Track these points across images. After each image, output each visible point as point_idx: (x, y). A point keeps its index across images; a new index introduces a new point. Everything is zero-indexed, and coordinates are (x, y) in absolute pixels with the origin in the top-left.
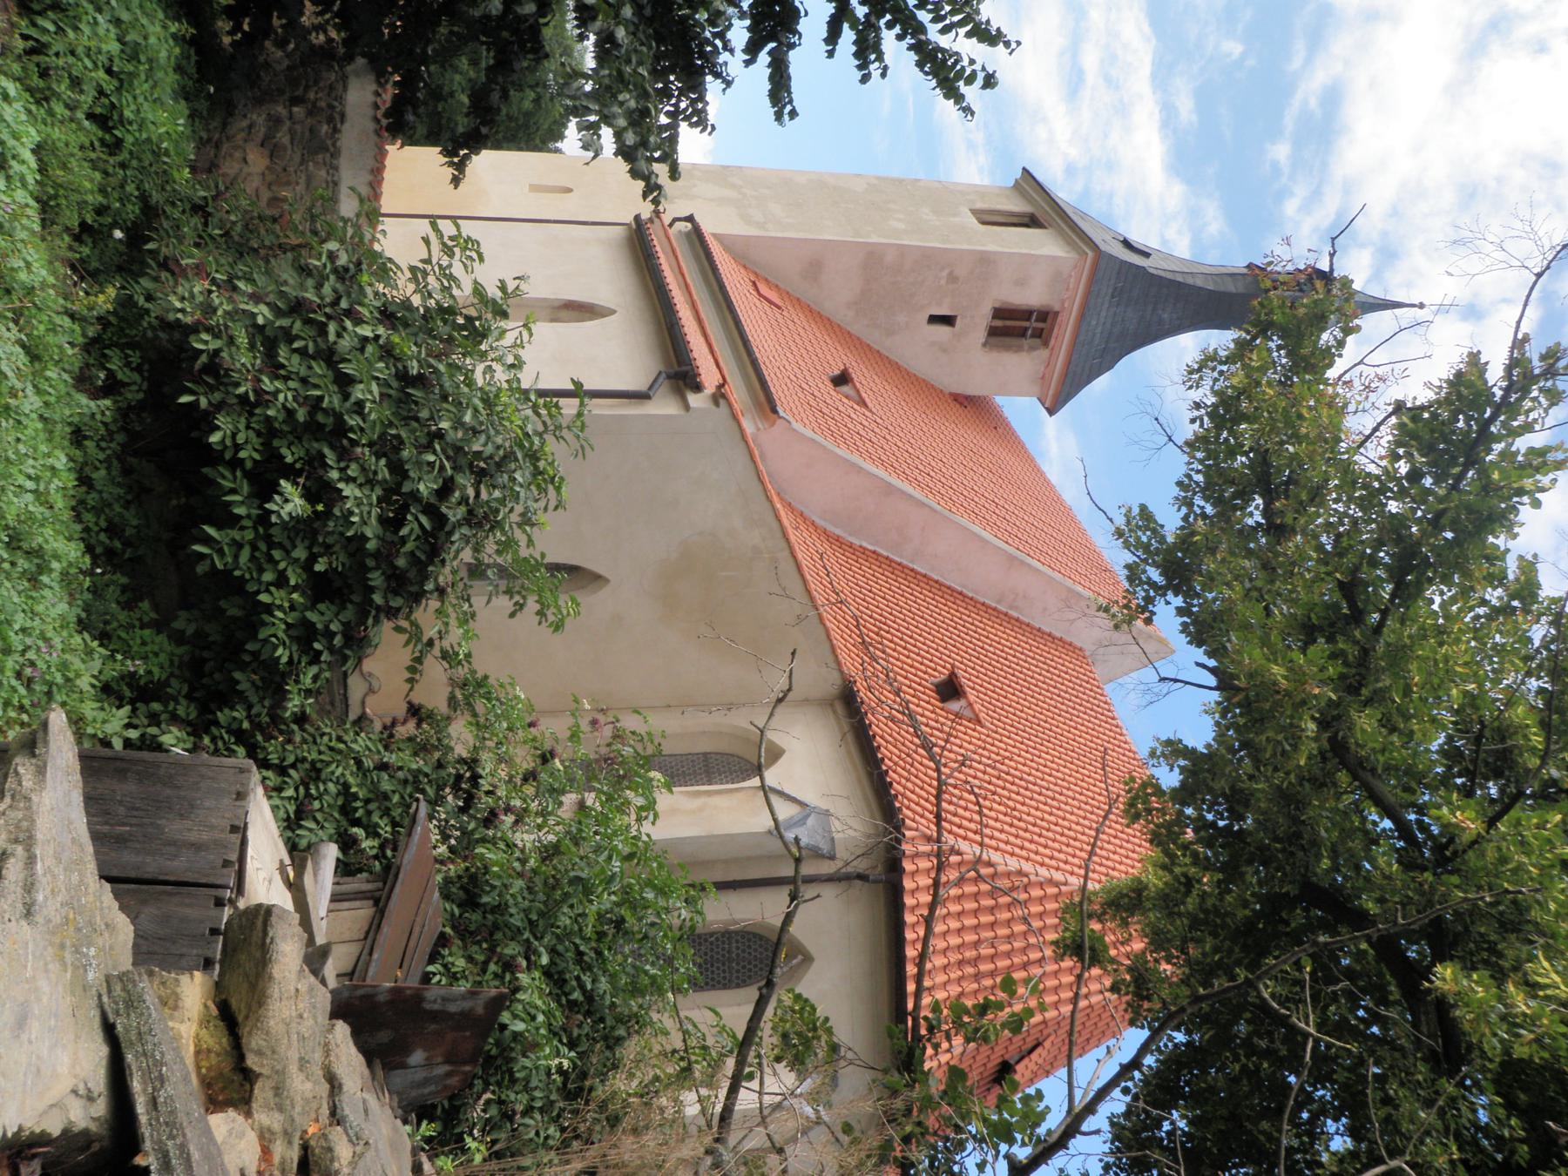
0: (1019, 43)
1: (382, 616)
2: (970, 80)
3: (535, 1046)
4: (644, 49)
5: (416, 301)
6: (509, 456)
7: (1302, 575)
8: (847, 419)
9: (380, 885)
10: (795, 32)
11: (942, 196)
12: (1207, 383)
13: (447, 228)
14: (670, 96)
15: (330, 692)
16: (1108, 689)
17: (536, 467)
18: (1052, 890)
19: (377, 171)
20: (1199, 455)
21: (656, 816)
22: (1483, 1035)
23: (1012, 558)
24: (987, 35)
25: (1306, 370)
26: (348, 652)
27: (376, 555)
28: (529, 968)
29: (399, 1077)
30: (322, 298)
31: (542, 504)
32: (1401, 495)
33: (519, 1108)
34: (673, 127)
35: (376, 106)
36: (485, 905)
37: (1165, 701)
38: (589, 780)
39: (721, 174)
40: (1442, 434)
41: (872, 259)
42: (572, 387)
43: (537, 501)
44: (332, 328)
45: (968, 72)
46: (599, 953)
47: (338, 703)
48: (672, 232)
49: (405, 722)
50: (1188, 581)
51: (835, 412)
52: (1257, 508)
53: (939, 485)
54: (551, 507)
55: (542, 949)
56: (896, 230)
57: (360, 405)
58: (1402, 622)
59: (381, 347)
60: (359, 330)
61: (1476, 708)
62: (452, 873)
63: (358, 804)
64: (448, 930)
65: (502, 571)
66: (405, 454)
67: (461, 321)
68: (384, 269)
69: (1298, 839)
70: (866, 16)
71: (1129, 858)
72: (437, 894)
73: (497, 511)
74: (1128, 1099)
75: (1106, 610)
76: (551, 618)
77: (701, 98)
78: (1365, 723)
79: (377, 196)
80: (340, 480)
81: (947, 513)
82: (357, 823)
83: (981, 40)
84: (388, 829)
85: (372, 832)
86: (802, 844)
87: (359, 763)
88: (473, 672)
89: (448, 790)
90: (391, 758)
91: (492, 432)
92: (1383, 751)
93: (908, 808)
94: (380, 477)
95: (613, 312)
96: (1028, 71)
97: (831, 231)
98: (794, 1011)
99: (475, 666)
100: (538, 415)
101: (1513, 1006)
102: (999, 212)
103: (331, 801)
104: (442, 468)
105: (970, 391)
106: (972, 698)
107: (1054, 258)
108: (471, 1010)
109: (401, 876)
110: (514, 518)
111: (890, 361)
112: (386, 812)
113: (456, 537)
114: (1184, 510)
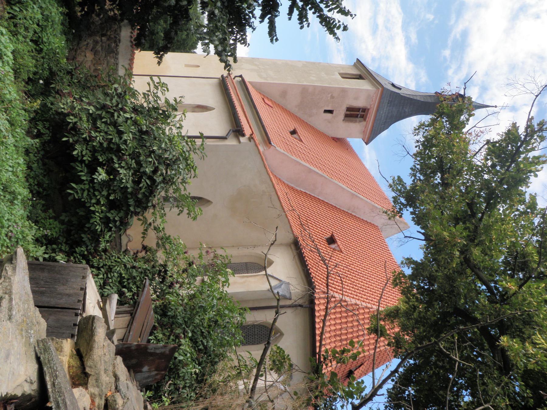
0: (355, 15)
1: (133, 215)
2: (338, 28)
3: (187, 365)
4: (225, 17)
5: (145, 105)
6: (178, 159)
7: (454, 200)
8: (295, 146)
9: (133, 308)
10: (277, 11)
11: (328, 68)
12: (421, 133)
13: (156, 79)
14: (234, 34)
15: (115, 241)
16: (387, 240)
17: (187, 163)
18: (367, 310)
19: (132, 60)
20: (418, 159)
21: (229, 284)
22: (517, 361)
23: (353, 195)
24: (344, 12)
25: (456, 129)
26: (121, 227)
27: (131, 193)
28: (184, 338)
29: (139, 376)
30: (112, 104)
31: (189, 176)
32: (489, 172)
33: (181, 386)
34: (235, 44)
35: (131, 37)
36: (169, 315)
37: (406, 245)
38: (205, 272)
39: (251, 61)
40: (503, 151)
41: (304, 90)
42: (199, 135)
43: (187, 175)
44: (116, 114)
45: (338, 25)
46: (209, 332)
47: (118, 245)
48: (234, 81)
49: (141, 252)
50: (414, 203)
51: (291, 144)
52: (438, 177)
53: (328, 169)
54: (192, 177)
55: (189, 331)
56: (313, 80)
57: (125, 141)
58: (489, 217)
59: (133, 121)
60: (125, 115)
61: (515, 247)
62: (158, 305)
63: (125, 280)
64: (156, 324)
65: (175, 199)
66: (141, 158)
67: (161, 112)
68: (134, 94)
69: (453, 293)
70: (302, 5)
71: (394, 299)
72: (152, 312)
73: (174, 178)
74: (394, 383)
75: (386, 213)
76: (192, 216)
77: (245, 34)
78: (476, 252)
79: (131, 68)
80: (119, 167)
81: (330, 179)
82: (124, 287)
83: (342, 14)
84: (135, 289)
85: (130, 290)
86: (280, 294)
87: (125, 266)
88: (165, 234)
89: (156, 275)
90: (136, 264)
91: (172, 151)
92: (482, 262)
93: (317, 282)
94: (133, 166)
95: (214, 109)
96: (359, 25)
97: (290, 81)
98: (277, 353)
99: (166, 232)
100: (188, 145)
101: (528, 351)
102: (348, 74)
103: (116, 279)
104: (154, 163)
105: (338, 136)
106: (339, 243)
107: (368, 90)
108: (164, 352)
109: (140, 305)
110: (179, 180)
111: (310, 126)
112: (135, 283)
113: (159, 187)
114: (413, 178)
